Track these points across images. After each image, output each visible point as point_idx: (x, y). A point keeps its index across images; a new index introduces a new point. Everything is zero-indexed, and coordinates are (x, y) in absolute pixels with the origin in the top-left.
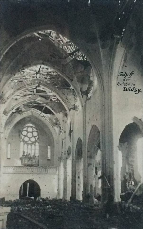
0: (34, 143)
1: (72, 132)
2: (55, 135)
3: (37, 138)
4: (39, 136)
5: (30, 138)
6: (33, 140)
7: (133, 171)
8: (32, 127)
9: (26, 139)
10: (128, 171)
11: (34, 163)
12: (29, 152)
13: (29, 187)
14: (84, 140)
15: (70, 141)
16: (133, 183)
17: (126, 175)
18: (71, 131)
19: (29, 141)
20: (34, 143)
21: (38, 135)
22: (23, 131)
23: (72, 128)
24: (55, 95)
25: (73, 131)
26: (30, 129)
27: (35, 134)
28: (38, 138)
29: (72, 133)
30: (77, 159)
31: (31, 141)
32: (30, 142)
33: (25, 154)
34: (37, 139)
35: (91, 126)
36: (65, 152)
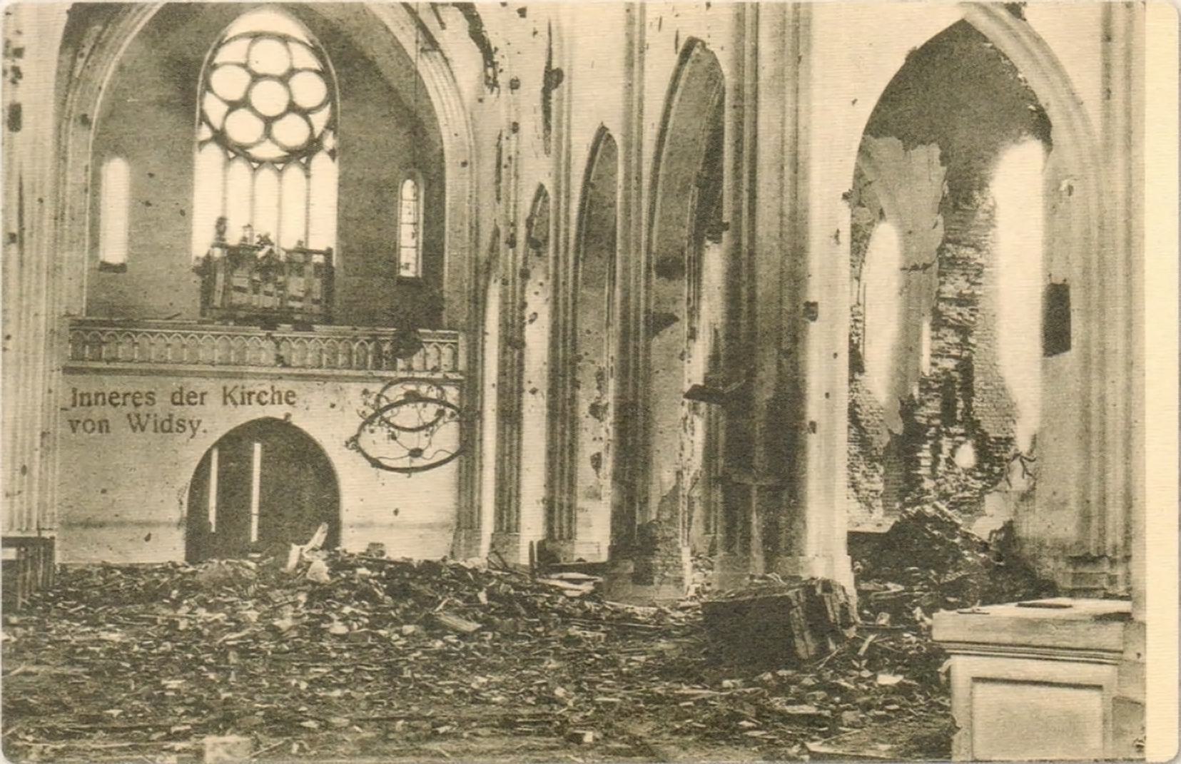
0: (302, 154)
1: (559, 81)
2: (688, 589)
3: (320, 120)
4: (334, 107)
5: (269, 121)
6: (293, 132)
7: (966, 367)
8: (284, 39)
9: (243, 128)
10: (935, 370)
11: (297, 305)
12: (264, 225)
13: (262, 476)
14: (738, 64)
15: (547, 152)
16: (966, 456)
17: (916, 392)
18: (553, 78)
19: (259, 143)
20: (302, 154)
21: (330, 98)
22: (214, 67)
23: (561, 56)
24: (507, 242)
25: (565, 83)
26: (270, 58)
27: (310, 90)
28: (331, 125)
29: (554, 93)
30: (344, 97)
31: (275, 142)
32: (267, 151)
33: (233, 238)
34: (319, 129)
35: (677, 47)
36: (1105, 162)
